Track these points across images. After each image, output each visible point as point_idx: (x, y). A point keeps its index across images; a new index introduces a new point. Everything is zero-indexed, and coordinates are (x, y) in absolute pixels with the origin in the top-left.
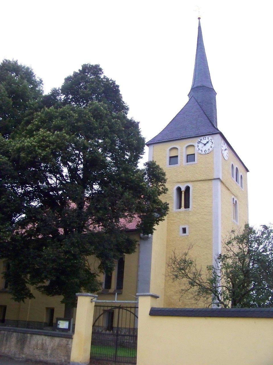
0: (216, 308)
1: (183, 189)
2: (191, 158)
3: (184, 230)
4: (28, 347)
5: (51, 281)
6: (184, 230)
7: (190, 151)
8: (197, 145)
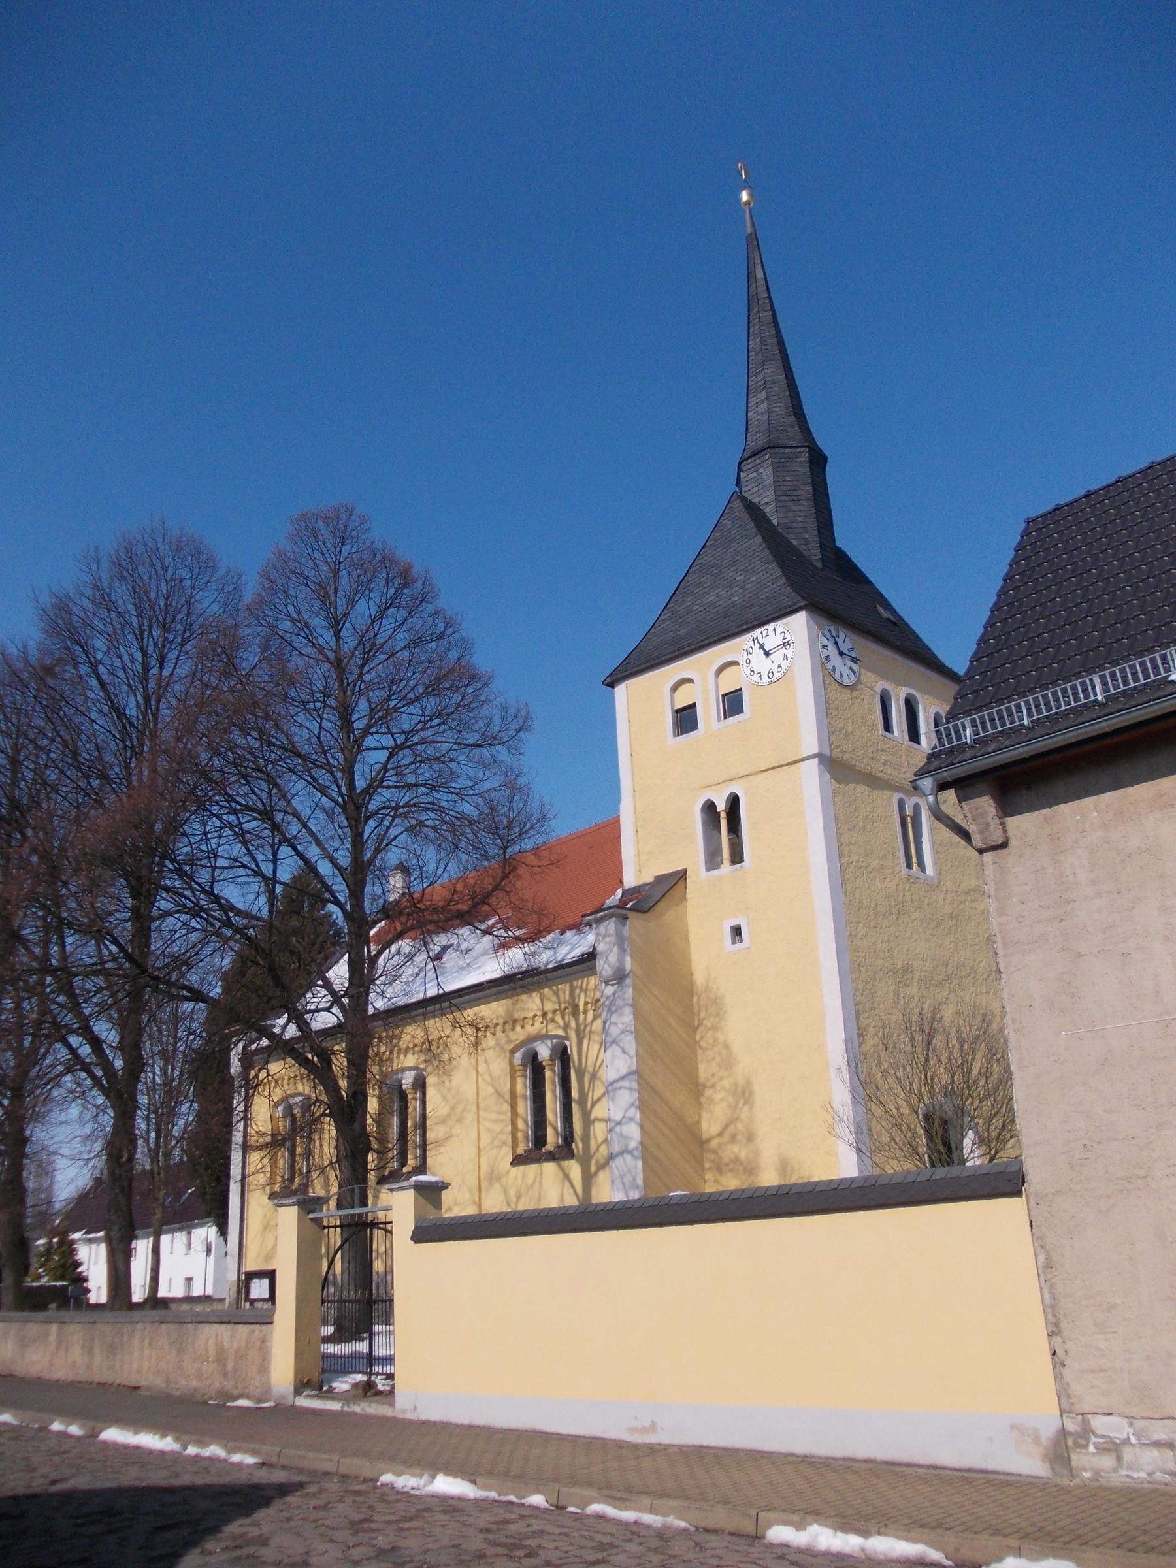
0: (346, 968)
1: (721, 806)
2: (733, 703)
3: (737, 931)
4: (97, 831)
5: (222, 979)
6: (737, 931)
7: (728, 684)
8: (746, 657)
